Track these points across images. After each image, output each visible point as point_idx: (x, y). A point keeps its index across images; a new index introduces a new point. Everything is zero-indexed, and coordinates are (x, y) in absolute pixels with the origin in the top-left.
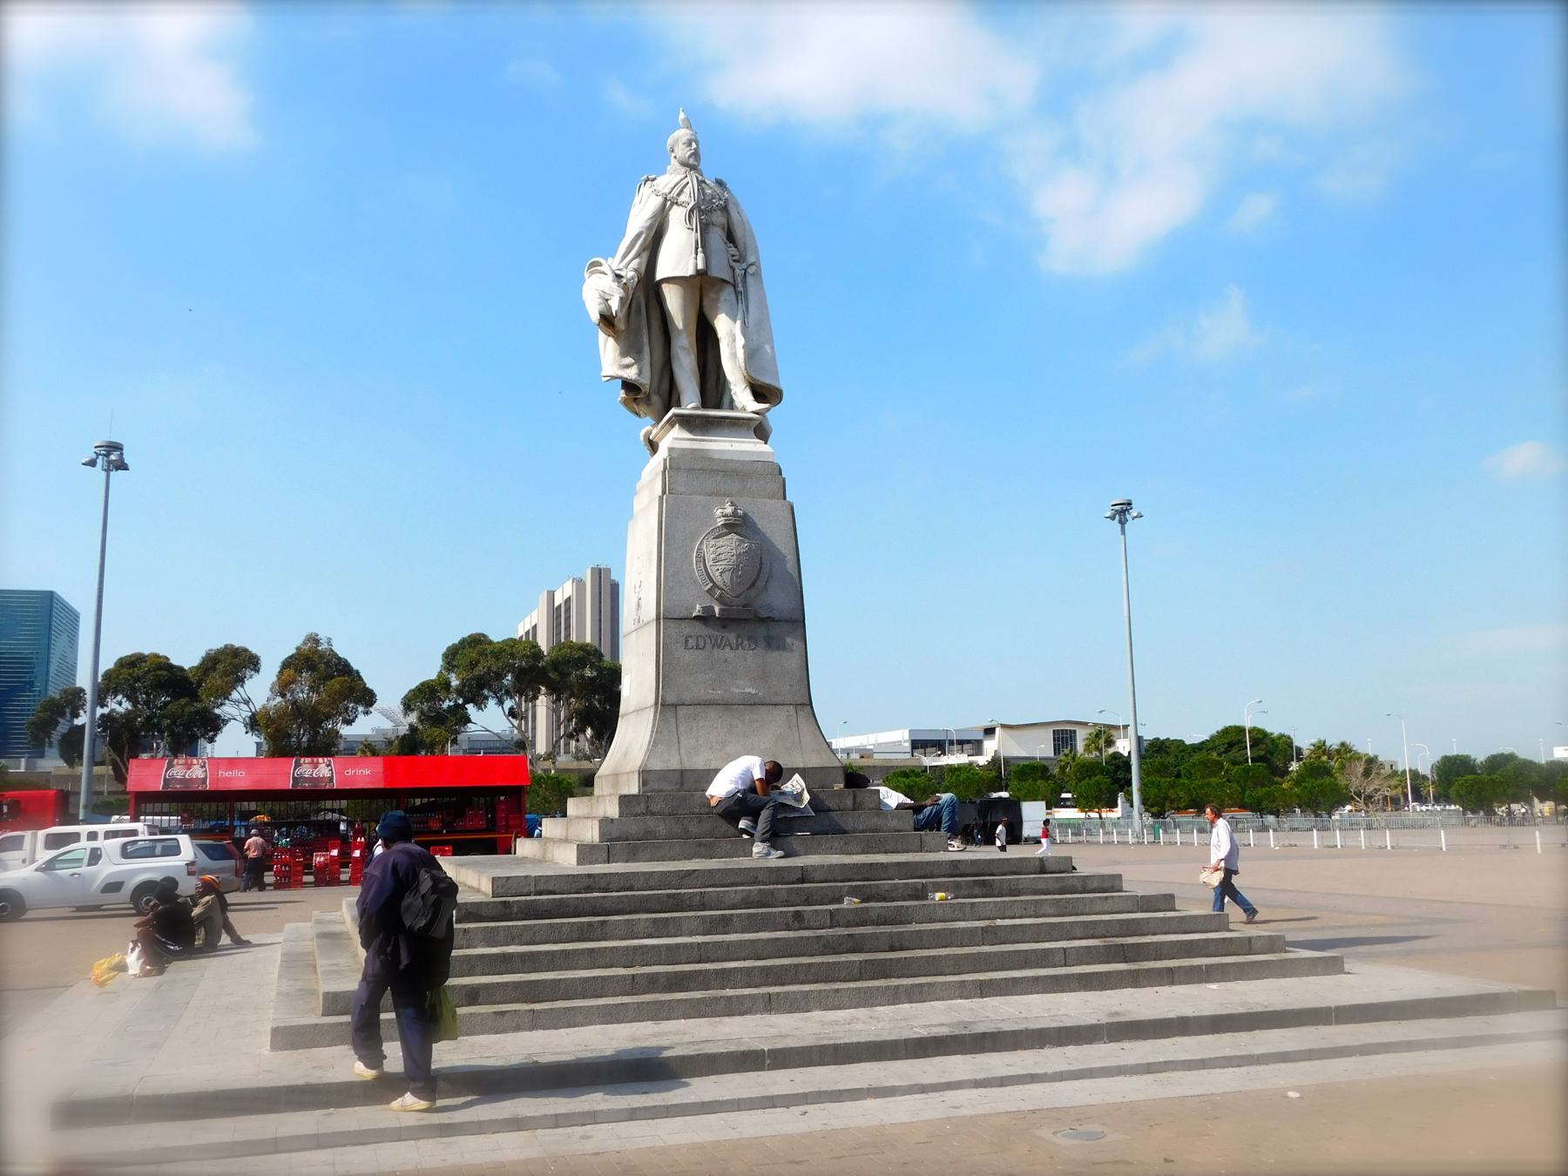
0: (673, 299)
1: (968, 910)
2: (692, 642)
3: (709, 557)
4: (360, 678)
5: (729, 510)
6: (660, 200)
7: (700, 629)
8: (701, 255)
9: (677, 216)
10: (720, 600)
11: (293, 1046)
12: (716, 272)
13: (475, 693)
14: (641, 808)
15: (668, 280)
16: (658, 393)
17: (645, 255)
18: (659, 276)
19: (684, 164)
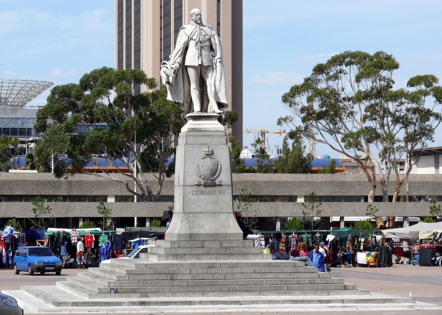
0: (192, 73)
1: (253, 266)
2: (194, 193)
3: (200, 165)
4: (414, 78)
5: (207, 150)
6: (187, 38)
7: (196, 188)
8: (200, 59)
9: (192, 44)
10: (203, 179)
11: (120, 201)
12: (205, 64)
13: (138, 113)
14: (177, 246)
15: (190, 66)
16: (186, 102)
17: (182, 56)
18: (186, 64)
19: (196, 22)
